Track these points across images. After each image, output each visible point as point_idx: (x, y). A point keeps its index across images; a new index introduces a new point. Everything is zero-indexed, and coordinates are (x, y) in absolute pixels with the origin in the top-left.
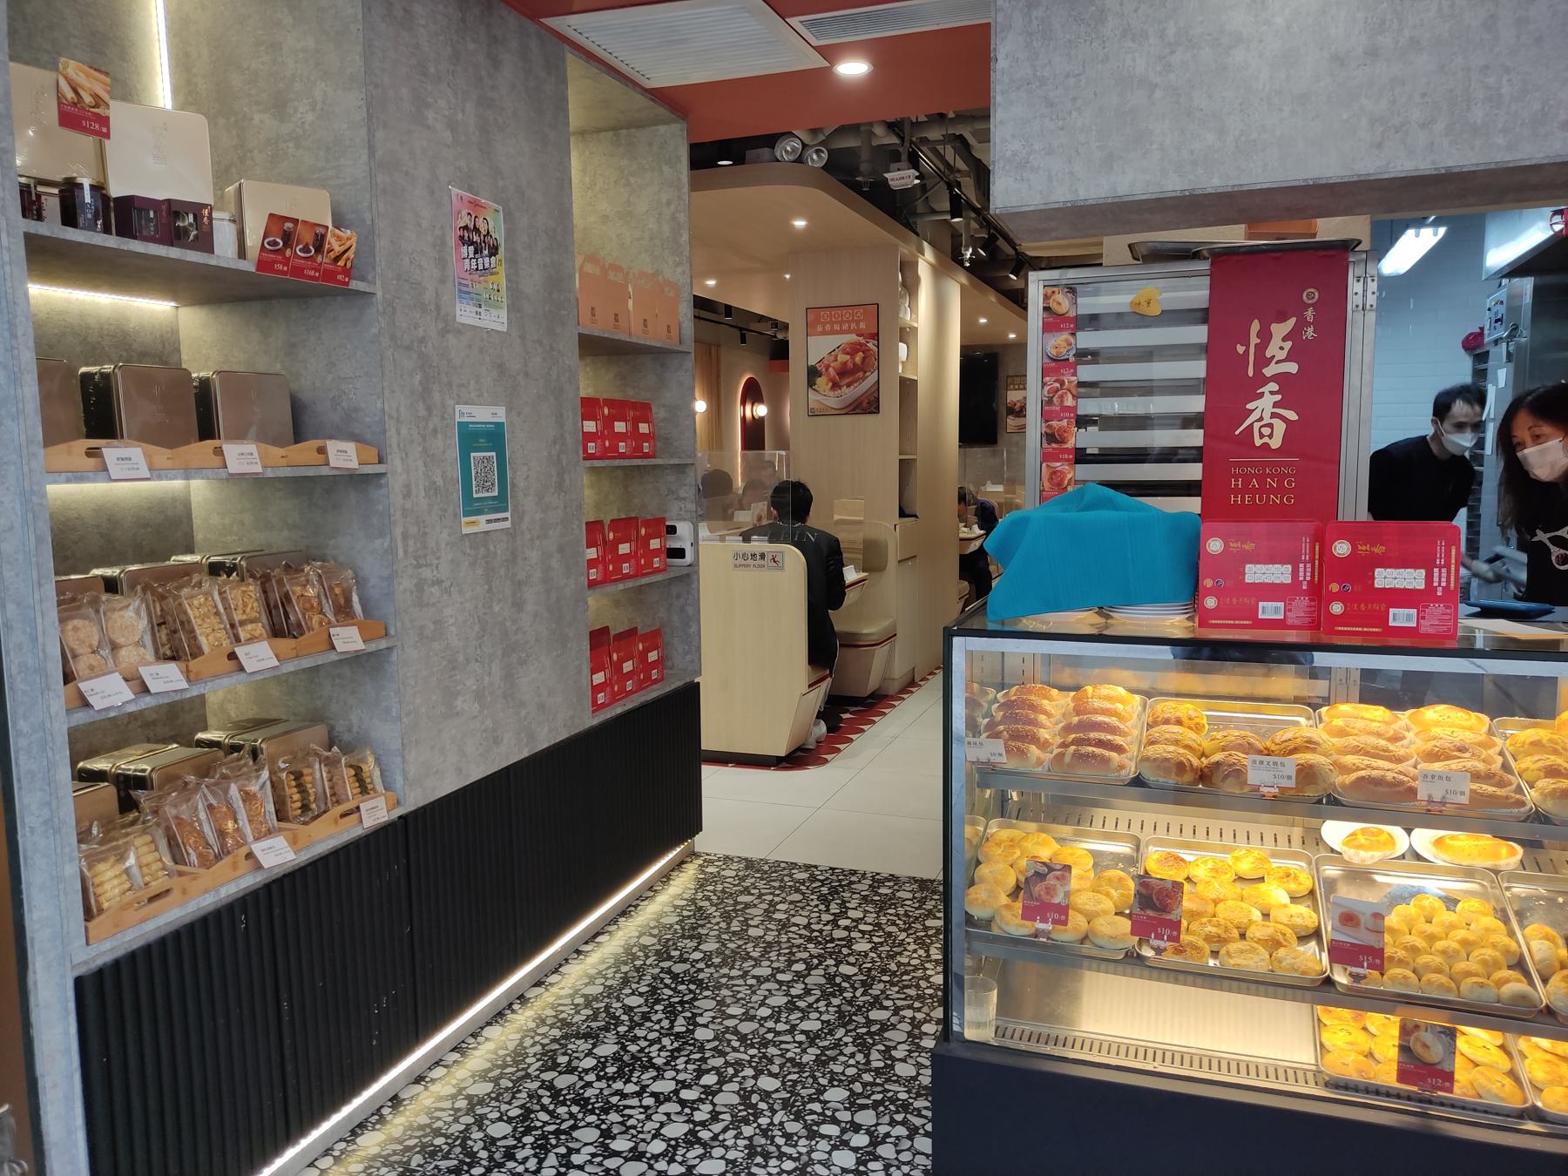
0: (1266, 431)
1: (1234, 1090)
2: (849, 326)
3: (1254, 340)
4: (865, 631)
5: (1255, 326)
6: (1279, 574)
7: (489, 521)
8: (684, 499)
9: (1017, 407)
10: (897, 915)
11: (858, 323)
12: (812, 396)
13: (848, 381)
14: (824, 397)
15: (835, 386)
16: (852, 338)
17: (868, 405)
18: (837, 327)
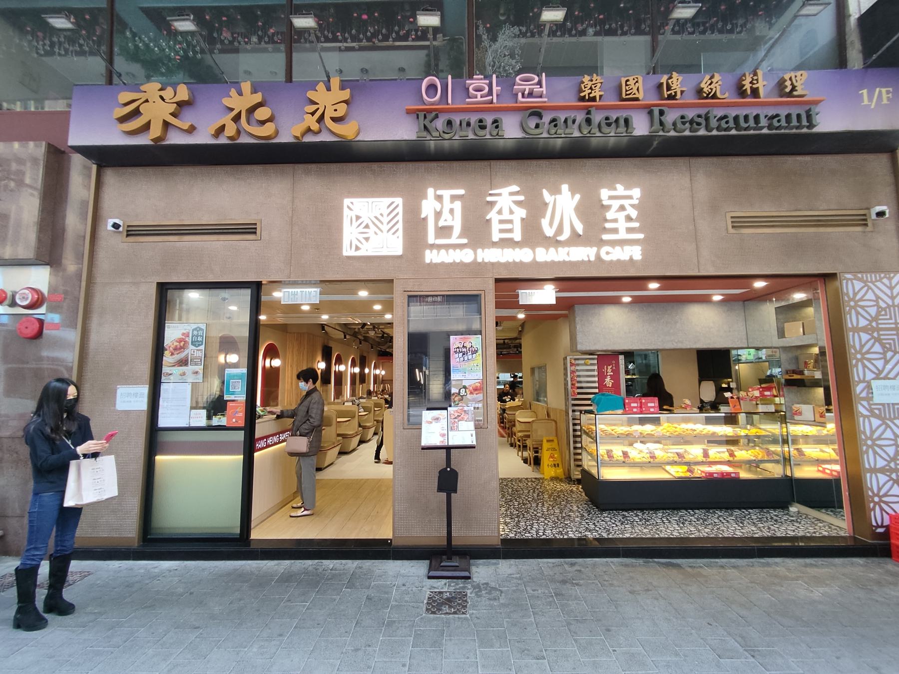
1: (868, 302)
6: (635, 405)
15: (172, 354)
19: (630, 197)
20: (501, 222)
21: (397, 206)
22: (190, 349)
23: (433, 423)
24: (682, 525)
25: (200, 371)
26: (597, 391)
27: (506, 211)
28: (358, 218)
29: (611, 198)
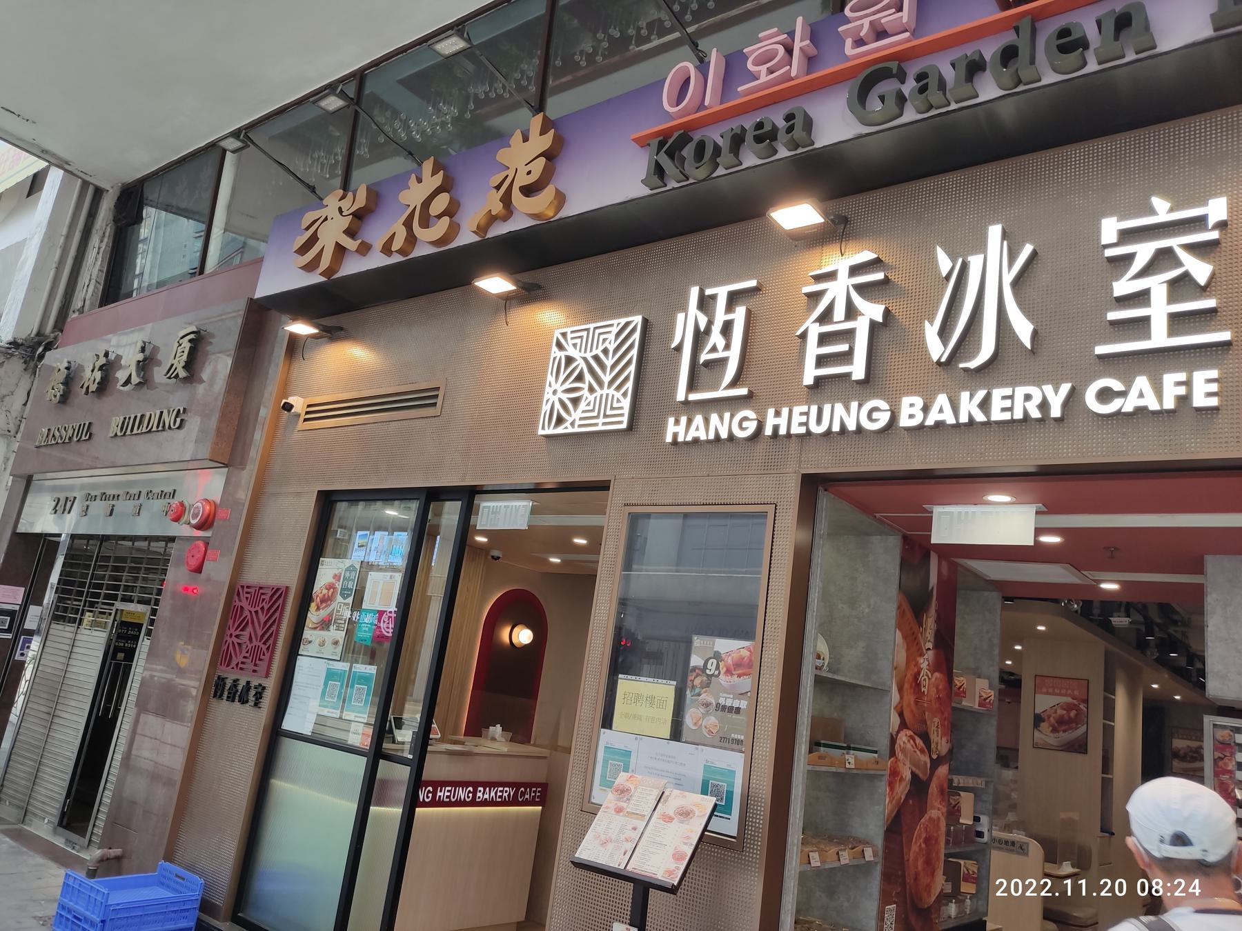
2: (1066, 692)
4: (1075, 914)
8: (985, 802)
9: (1182, 753)
11: (1073, 690)
12: (1037, 734)
13: (740, 672)
14: (1045, 735)
15: (1055, 730)
16: (1069, 700)
17: (1079, 747)
18: (1057, 691)
19: (1198, 223)
22: (338, 601)
25: (340, 640)
27: (839, 312)
28: (569, 360)
29: (1127, 236)
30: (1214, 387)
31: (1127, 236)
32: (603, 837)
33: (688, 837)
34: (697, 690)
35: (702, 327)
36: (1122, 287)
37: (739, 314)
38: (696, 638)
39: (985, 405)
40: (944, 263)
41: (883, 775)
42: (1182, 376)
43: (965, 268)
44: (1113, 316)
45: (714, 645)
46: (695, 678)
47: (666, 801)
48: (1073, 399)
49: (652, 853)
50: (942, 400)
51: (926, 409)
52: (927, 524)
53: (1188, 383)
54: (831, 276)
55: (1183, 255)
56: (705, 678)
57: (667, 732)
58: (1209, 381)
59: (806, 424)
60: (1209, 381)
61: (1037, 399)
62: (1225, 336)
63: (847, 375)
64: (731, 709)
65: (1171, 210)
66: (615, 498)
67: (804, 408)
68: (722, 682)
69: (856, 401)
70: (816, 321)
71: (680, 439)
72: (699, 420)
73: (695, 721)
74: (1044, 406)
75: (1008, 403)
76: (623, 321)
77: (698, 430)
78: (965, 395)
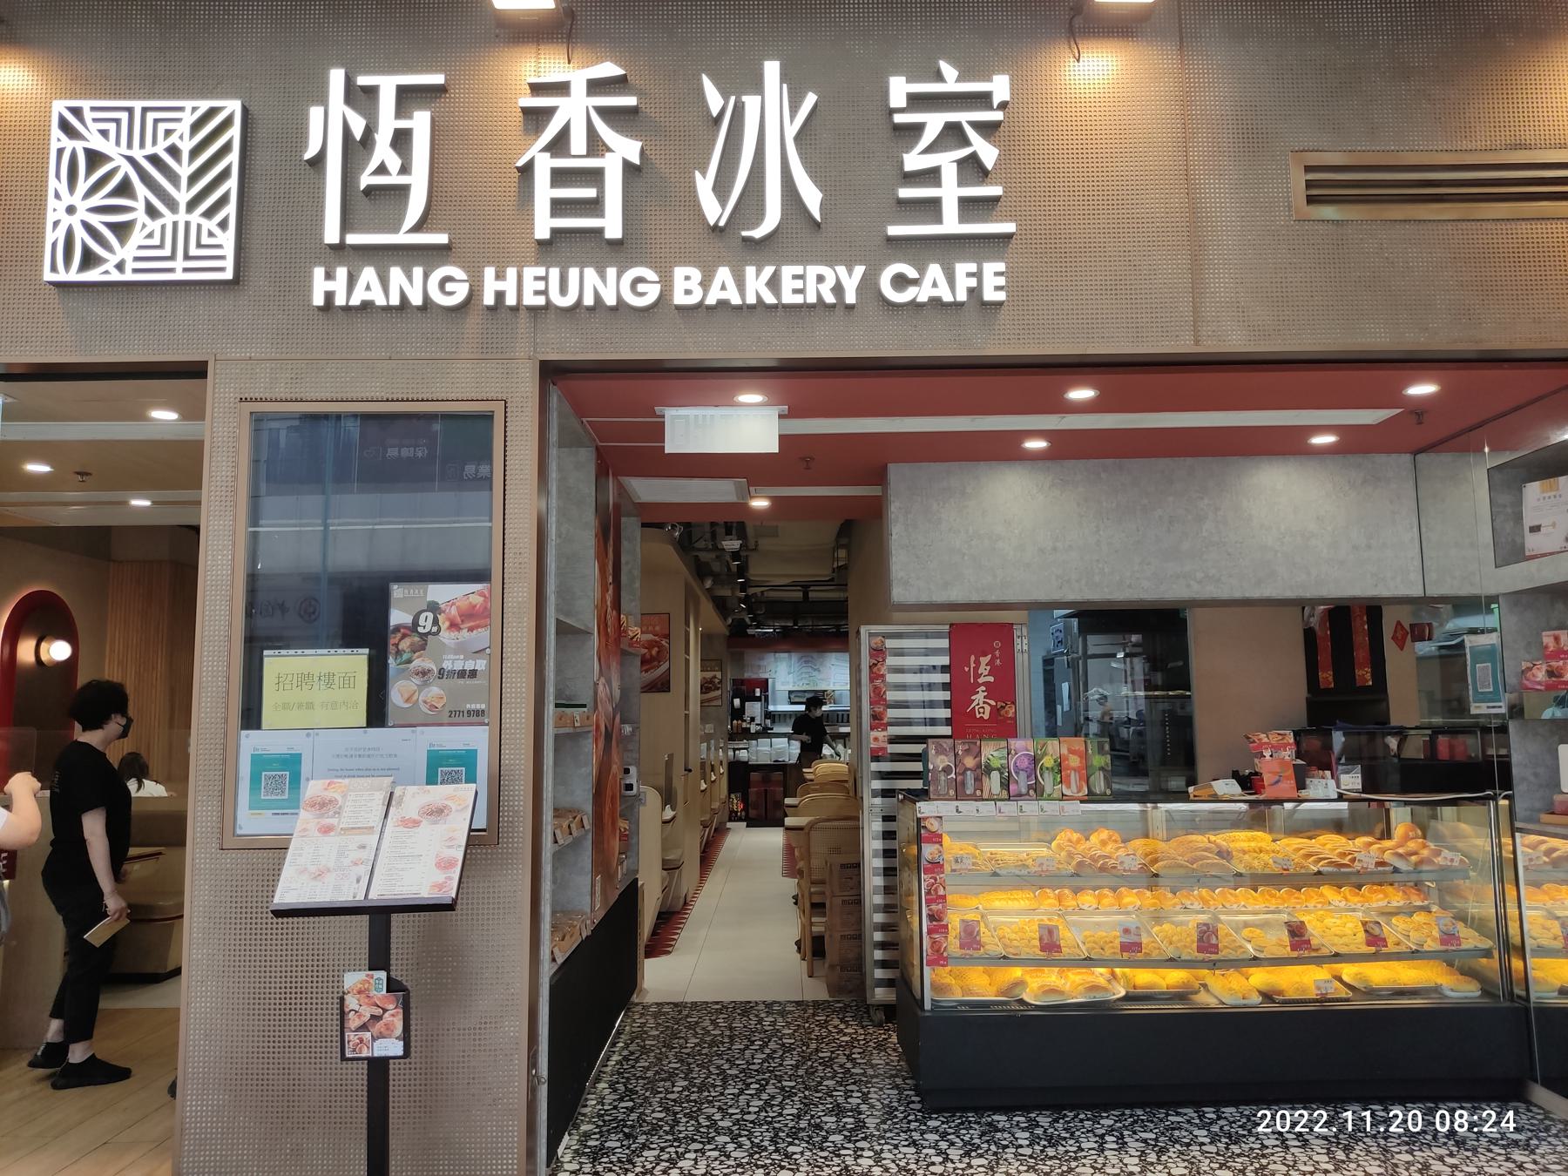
0: (981, 710)
3: (973, 665)
5: (973, 658)
7: (1488, 707)
8: (632, 751)
10: (611, 1162)
13: (472, 624)
16: (650, 637)
19: (983, 100)
20: (560, 177)
21: (227, 123)
23: (424, 823)
24: (1341, 1155)
26: (947, 730)
27: (578, 143)
28: (95, 158)
29: (917, 102)
30: (1001, 281)
31: (917, 102)
32: (313, 869)
33: (451, 839)
34: (405, 657)
35: (358, 130)
36: (914, 161)
37: (420, 122)
38: (395, 587)
39: (774, 283)
40: (714, 100)
41: (589, 732)
42: (973, 267)
43: (739, 111)
44: (905, 193)
45: (425, 593)
46: (400, 640)
47: (399, 803)
48: (869, 286)
49: (403, 870)
50: (724, 274)
51: (705, 284)
52: (658, 431)
53: (978, 275)
54: (562, 88)
55: (971, 133)
56: (417, 639)
57: (361, 716)
58: (997, 274)
59: (545, 292)
60: (997, 274)
61: (830, 281)
62: (1009, 227)
63: (599, 232)
64: (462, 674)
65: (958, 80)
66: (220, 390)
67: (541, 271)
68: (444, 640)
69: (321, 266)
70: (545, 150)
71: (340, 300)
72: (369, 274)
73: (406, 696)
74: (838, 289)
75: (799, 284)
76: (204, 105)
77: (368, 287)
78: (750, 271)
